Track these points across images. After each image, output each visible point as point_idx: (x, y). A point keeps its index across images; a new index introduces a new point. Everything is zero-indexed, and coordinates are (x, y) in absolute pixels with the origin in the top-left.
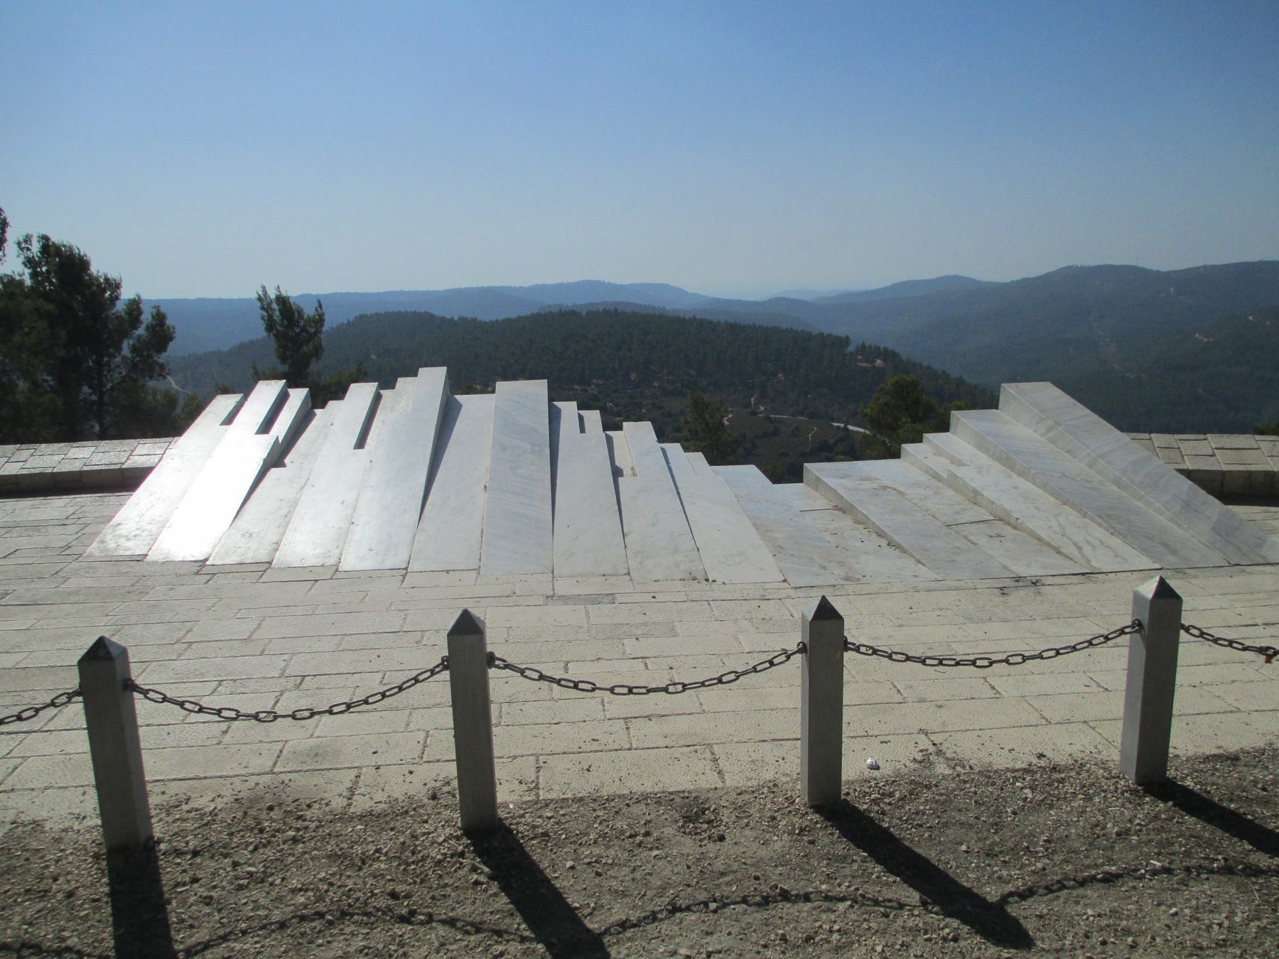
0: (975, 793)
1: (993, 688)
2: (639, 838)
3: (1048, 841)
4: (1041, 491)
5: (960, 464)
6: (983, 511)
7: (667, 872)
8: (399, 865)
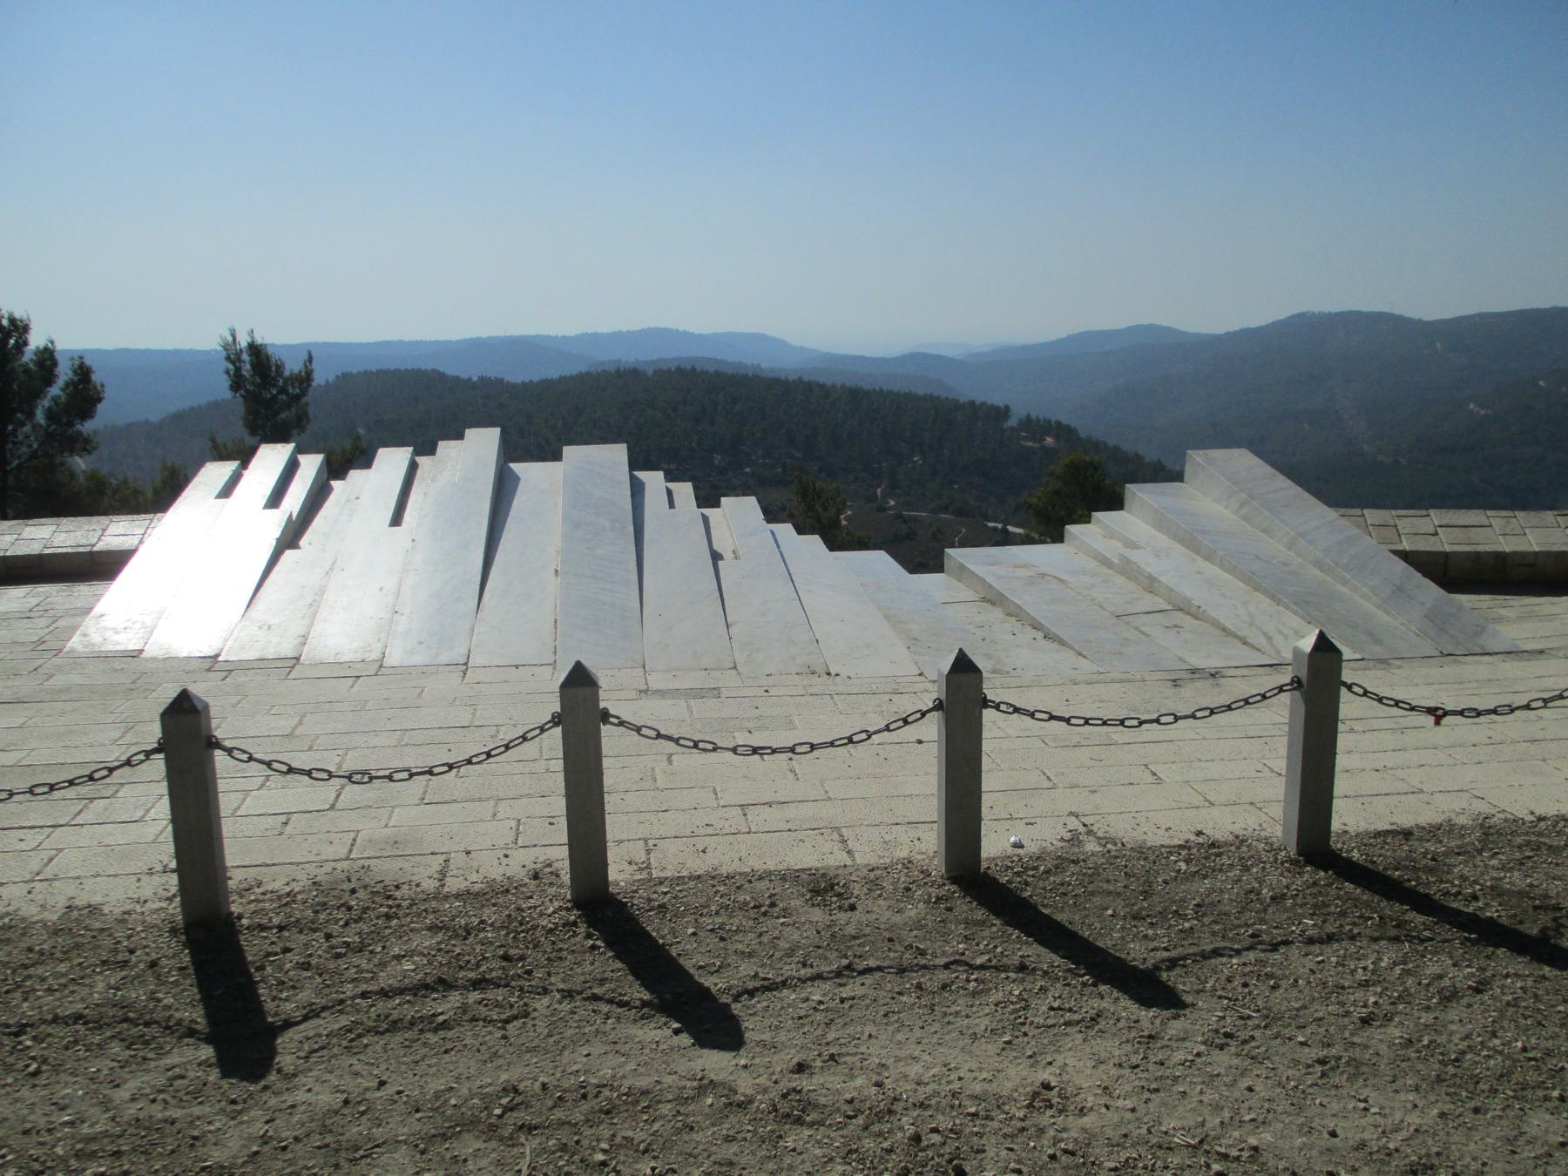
0: (1126, 866)
1: (1154, 774)
2: (763, 909)
3: (1198, 905)
4: (1228, 576)
5: (1133, 545)
6: (1161, 601)
7: (796, 937)
8: (508, 934)
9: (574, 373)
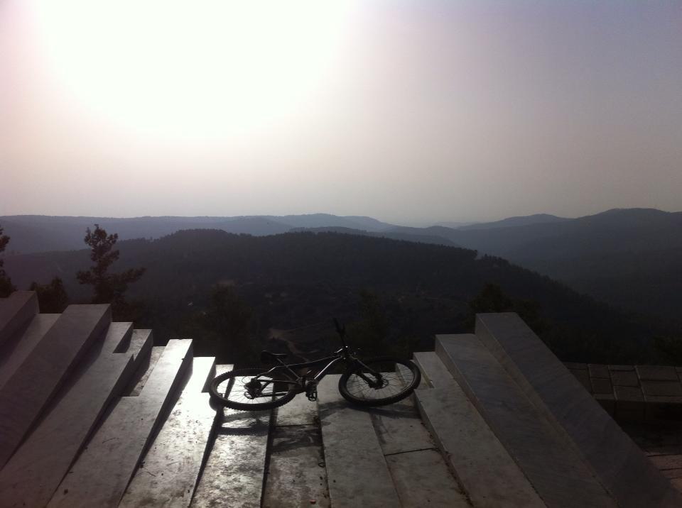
9: (368, 231)
